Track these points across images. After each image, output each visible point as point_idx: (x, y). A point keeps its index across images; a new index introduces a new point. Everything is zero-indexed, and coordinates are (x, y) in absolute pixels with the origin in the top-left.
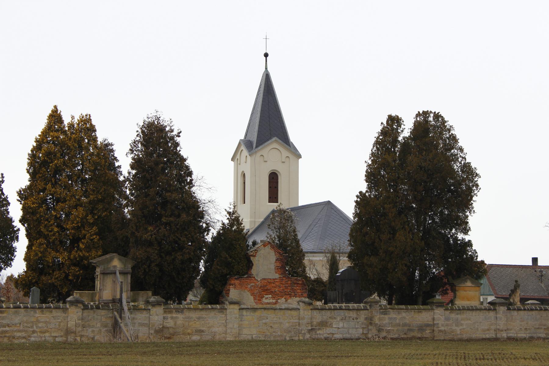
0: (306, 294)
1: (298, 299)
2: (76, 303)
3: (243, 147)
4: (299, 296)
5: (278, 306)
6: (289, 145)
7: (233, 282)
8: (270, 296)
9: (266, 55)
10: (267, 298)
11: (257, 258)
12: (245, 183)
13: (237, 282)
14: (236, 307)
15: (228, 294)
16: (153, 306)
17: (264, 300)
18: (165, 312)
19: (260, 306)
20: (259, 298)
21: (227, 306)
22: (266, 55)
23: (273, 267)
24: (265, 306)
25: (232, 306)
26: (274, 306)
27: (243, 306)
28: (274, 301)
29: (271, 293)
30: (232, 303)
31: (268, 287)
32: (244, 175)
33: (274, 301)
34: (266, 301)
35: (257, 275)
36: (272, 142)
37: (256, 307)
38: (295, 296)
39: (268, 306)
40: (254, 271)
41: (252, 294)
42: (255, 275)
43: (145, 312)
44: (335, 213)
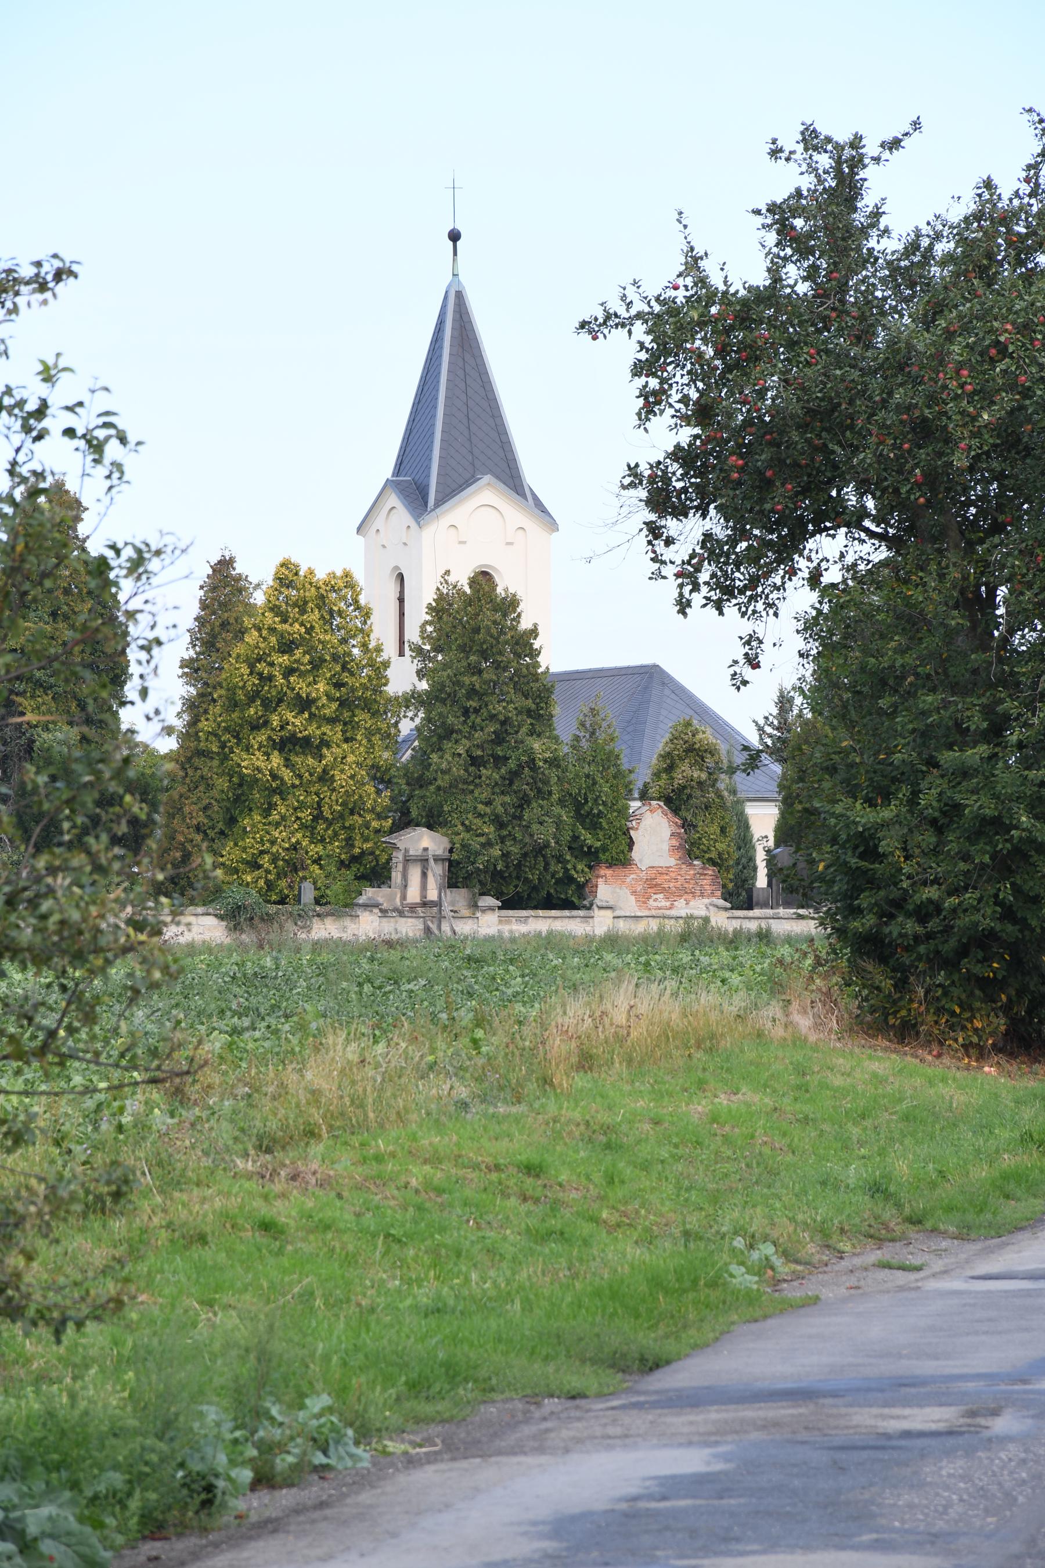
0: (719, 893)
1: (706, 901)
2: (368, 906)
3: (393, 500)
4: (708, 897)
5: (673, 913)
6: (523, 495)
7: (602, 872)
8: (661, 896)
9: (454, 236)
10: (656, 900)
11: (640, 831)
12: (401, 600)
13: (609, 872)
14: (608, 913)
15: (594, 893)
16: (483, 911)
17: (651, 902)
18: (500, 922)
19: (646, 913)
20: (643, 899)
21: (596, 912)
22: (454, 236)
23: (666, 847)
24: (654, 913)
25: (603, 912)
26: (667, 913)
27: (618, 913)
28: (668, 904)
29: (664, 890)
30: (600, 908)
31: (658, 881)
32: (401, 578)
33: (668, 904)
34: (655, 904)
35: (641, 861)
36: (480, 489)
37: (639, 914)
38: (702, 895)
39: (660, 912)
40: (635, 854)
41: (634, 893)
42: (637, 861)
43: (470, 921)
44: (673, 696)
